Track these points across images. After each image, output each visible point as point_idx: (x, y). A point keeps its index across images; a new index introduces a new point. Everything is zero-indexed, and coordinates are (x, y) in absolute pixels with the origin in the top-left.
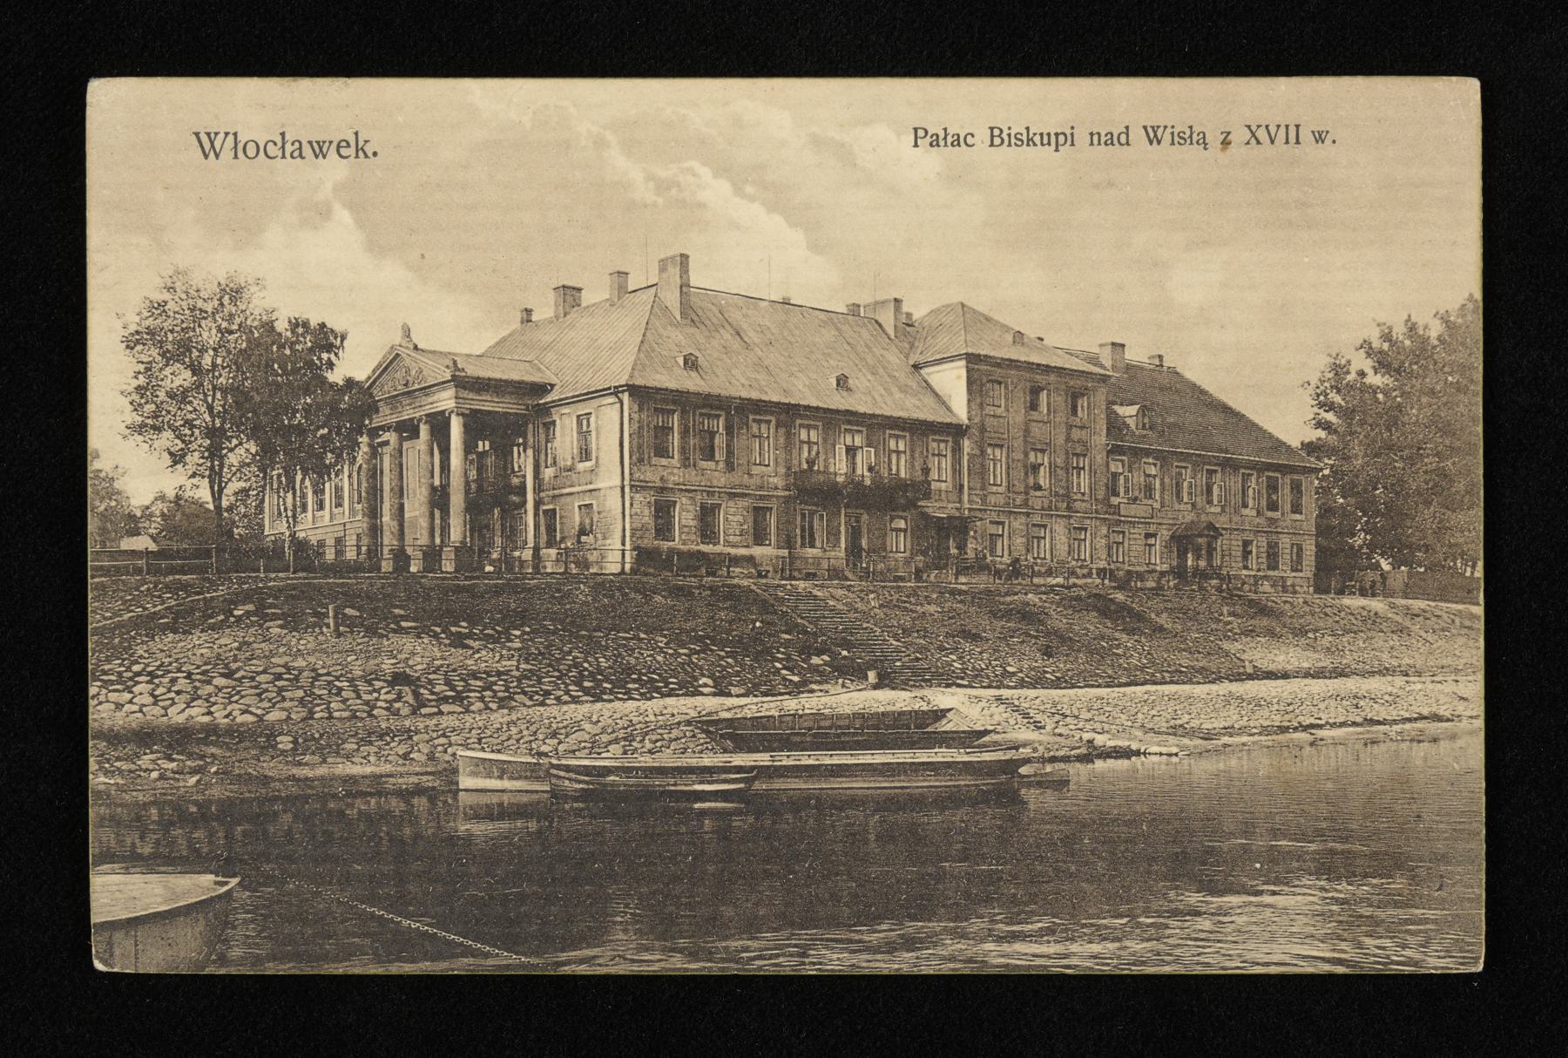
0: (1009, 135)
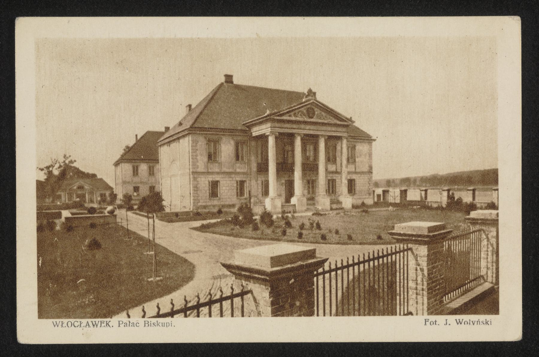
0: (151, 323)
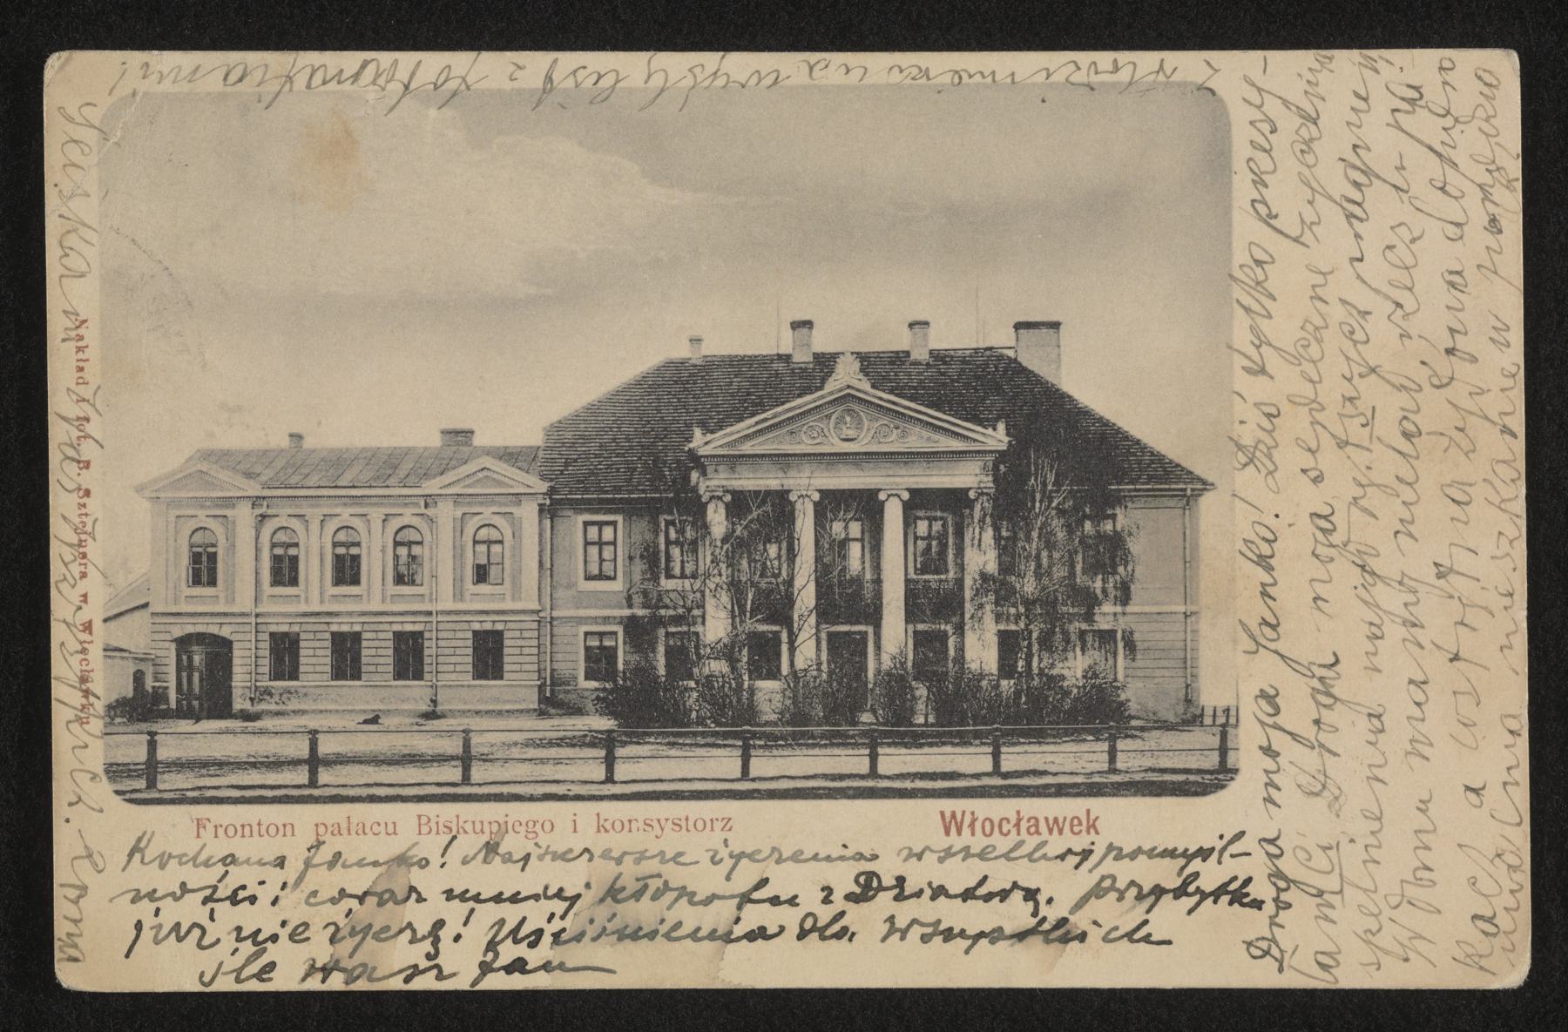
0: (437, 823)
